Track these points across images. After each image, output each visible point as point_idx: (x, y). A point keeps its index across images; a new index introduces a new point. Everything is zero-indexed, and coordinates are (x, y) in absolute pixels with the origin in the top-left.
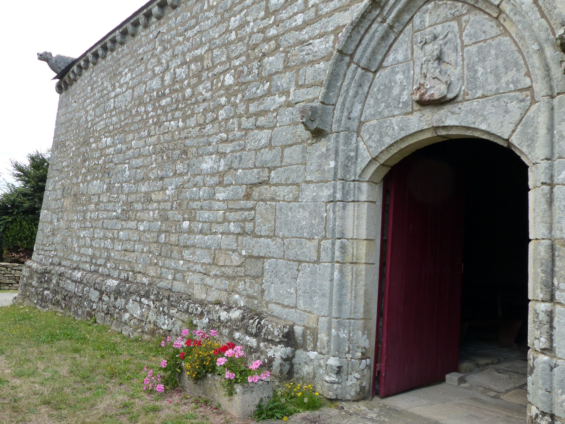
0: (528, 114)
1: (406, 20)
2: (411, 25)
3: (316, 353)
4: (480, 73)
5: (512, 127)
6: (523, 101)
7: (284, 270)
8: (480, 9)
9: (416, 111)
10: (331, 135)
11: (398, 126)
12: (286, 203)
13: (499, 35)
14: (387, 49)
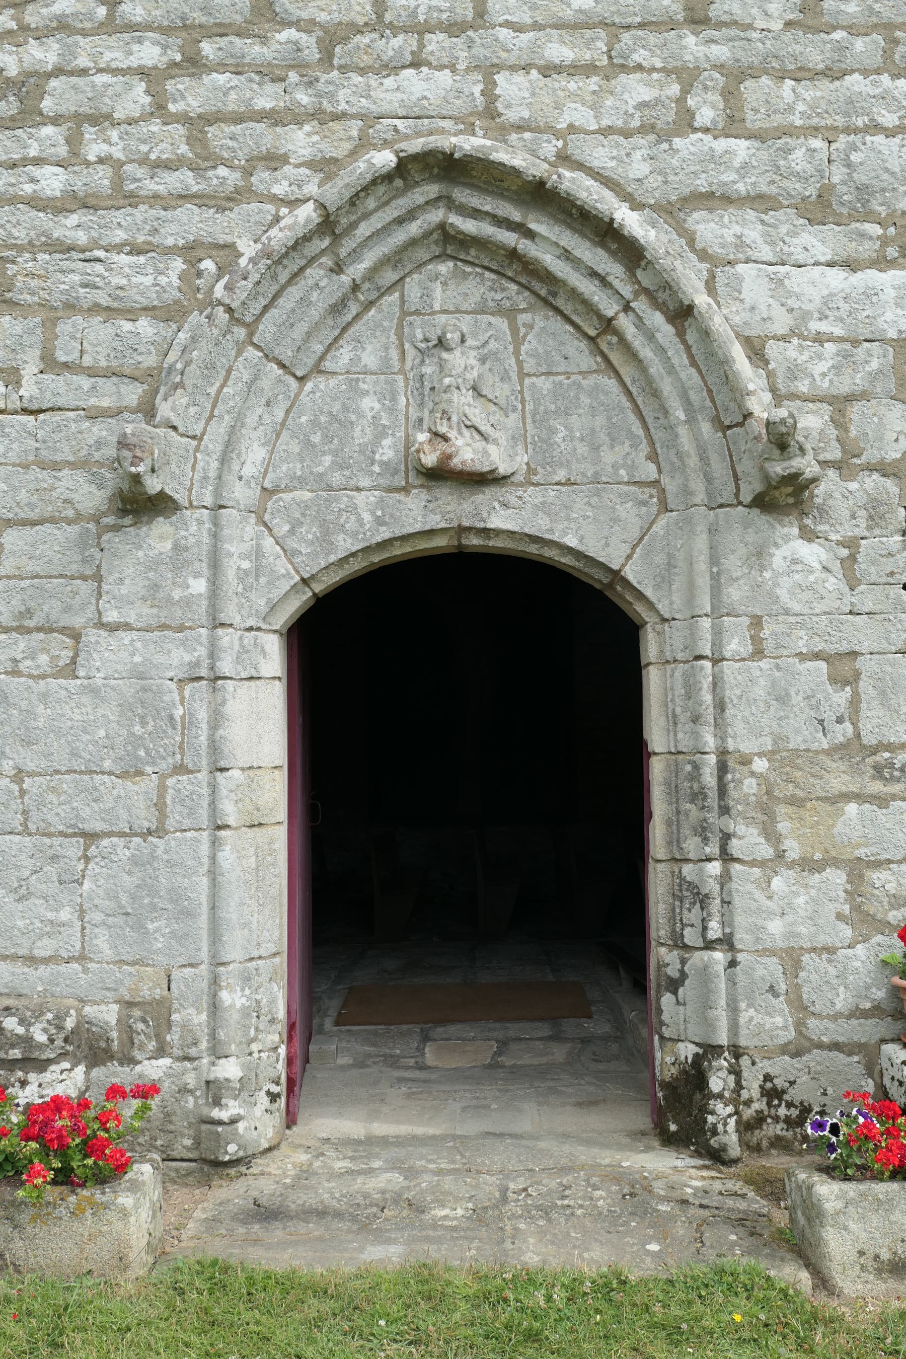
0: (654, 528)
1: (388, 283)
2: (397, 294)
3: (165, 1062)
4: (561, 435)
5: (626, 549)
6: (643, 503)
7: (29, 863)
8: (558, 311)
9: (415, 487)
10: (188, 512)
11: (373, 513)
12: (23, 679)
13: (595, 371)
14: (336, 332)
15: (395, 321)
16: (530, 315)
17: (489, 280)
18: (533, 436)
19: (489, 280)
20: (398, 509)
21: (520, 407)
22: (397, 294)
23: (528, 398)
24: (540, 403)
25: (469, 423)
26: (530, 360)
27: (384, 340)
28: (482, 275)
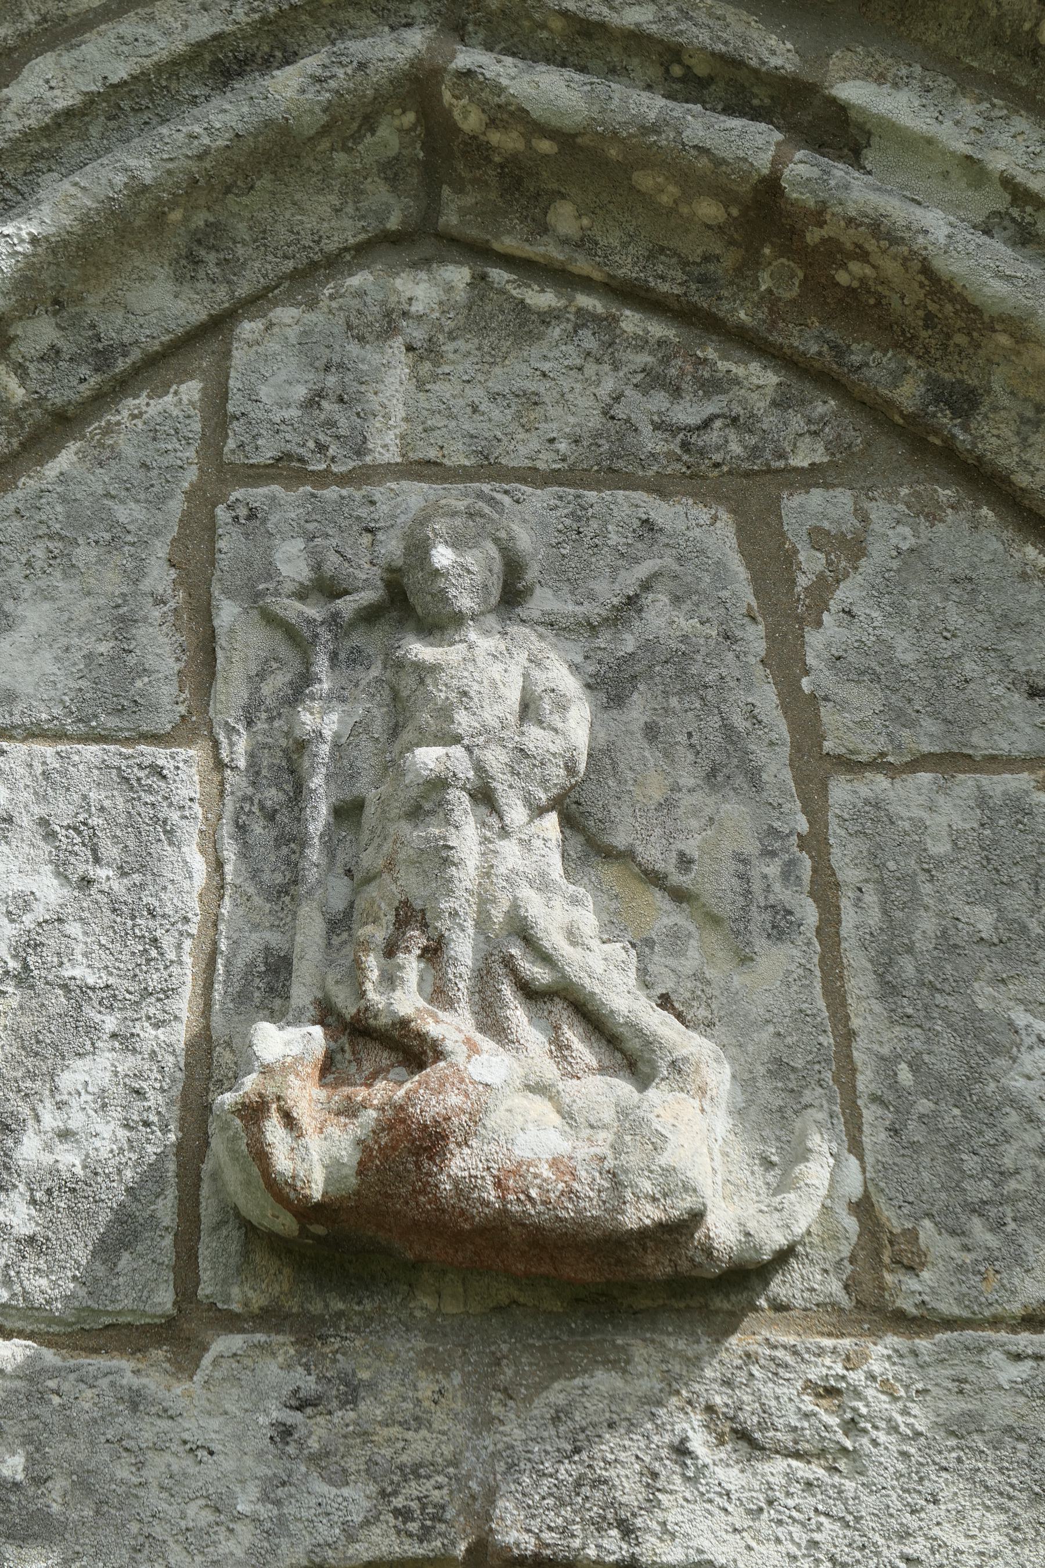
2: (191, 390)
9: (231, 1322)
15: (177, 505)
16: (844, 498)
17: (641, 343)
18: (887, 1064)
19: (641, 343)
20: (121, 1445)
21: (810, 914)
22: (191, 390)
23: (849, 874)
24: (914, 901)
25: (539, 974)
26: (852, 693)
27: (112, 583)
28: (607, 324)
